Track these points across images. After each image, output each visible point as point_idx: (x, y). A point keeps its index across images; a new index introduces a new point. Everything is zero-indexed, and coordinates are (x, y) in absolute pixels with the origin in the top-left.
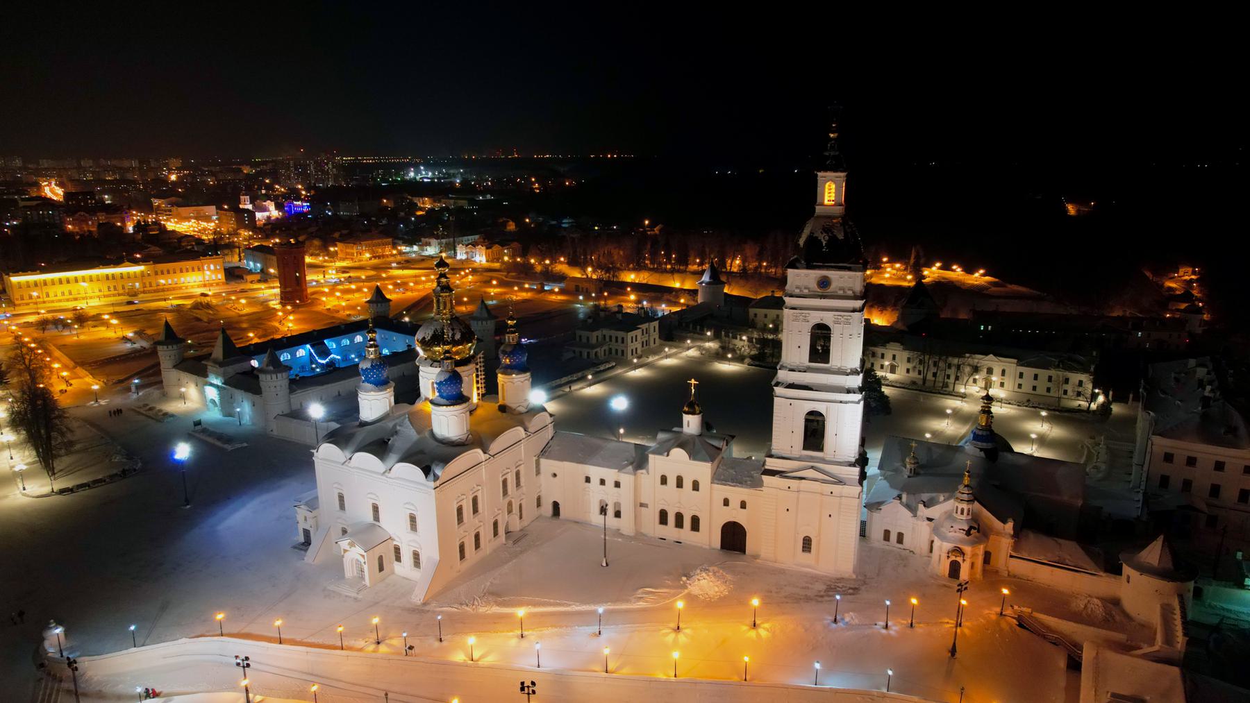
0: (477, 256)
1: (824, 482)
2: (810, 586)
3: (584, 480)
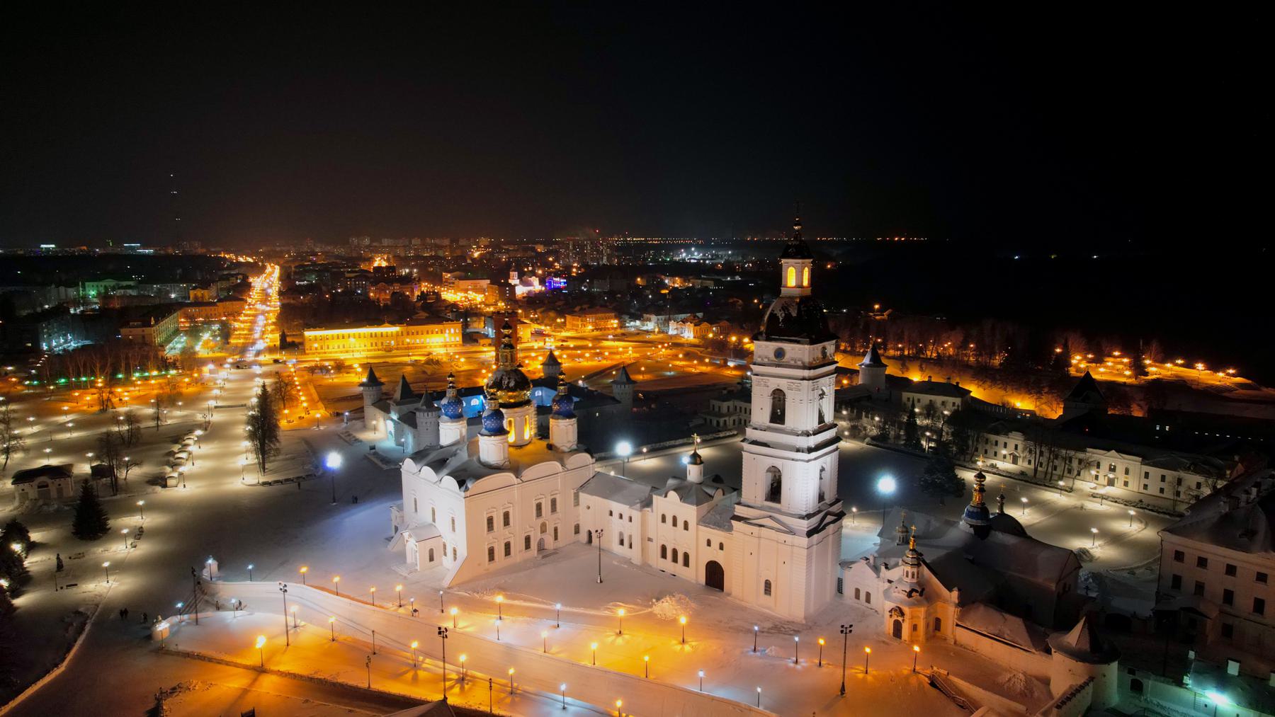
0: (686, 332)
1: (778, 530)
3: (608, 513)
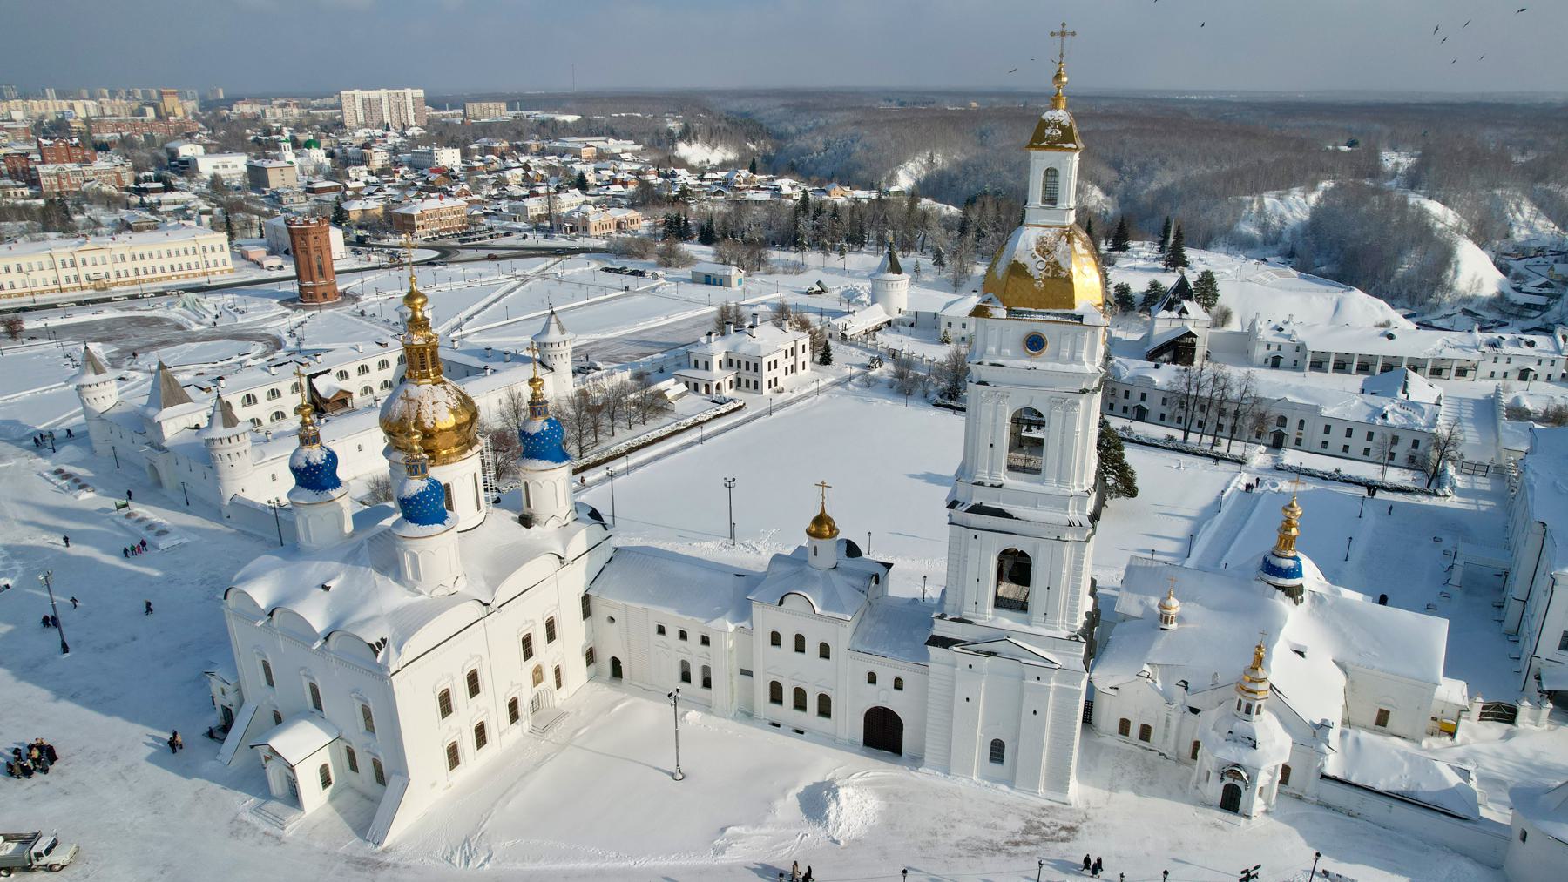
2: (999, 822)
